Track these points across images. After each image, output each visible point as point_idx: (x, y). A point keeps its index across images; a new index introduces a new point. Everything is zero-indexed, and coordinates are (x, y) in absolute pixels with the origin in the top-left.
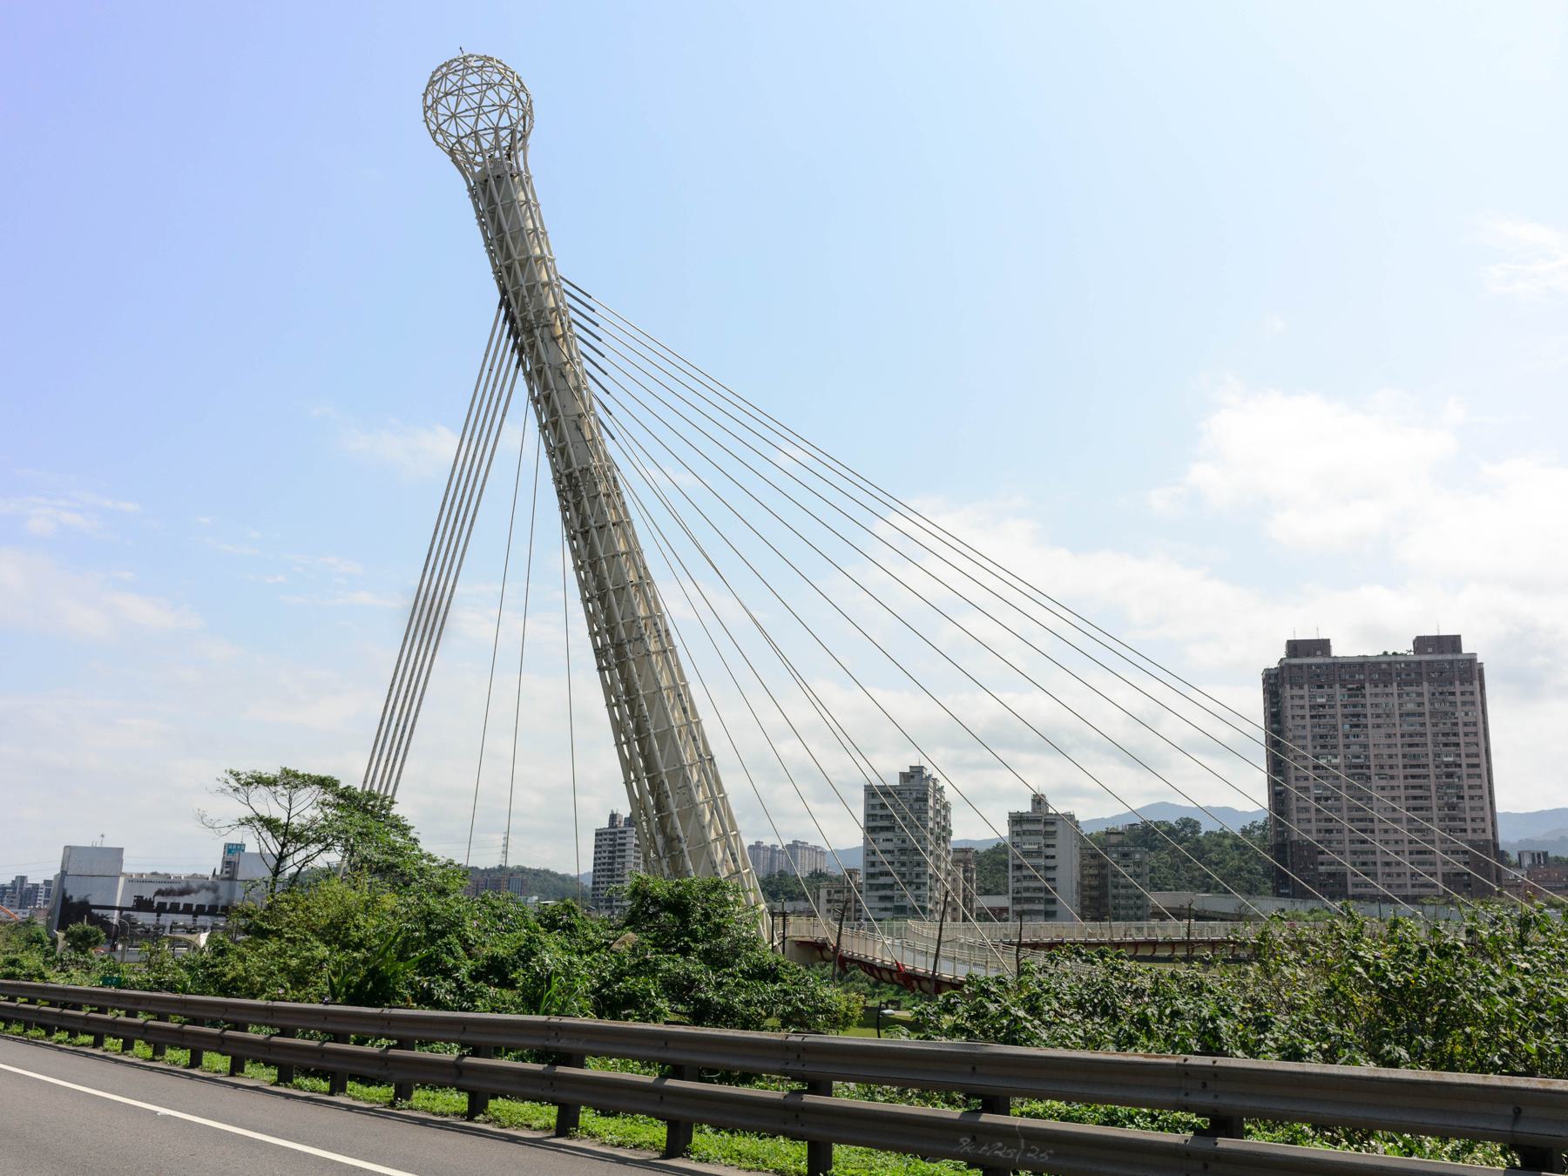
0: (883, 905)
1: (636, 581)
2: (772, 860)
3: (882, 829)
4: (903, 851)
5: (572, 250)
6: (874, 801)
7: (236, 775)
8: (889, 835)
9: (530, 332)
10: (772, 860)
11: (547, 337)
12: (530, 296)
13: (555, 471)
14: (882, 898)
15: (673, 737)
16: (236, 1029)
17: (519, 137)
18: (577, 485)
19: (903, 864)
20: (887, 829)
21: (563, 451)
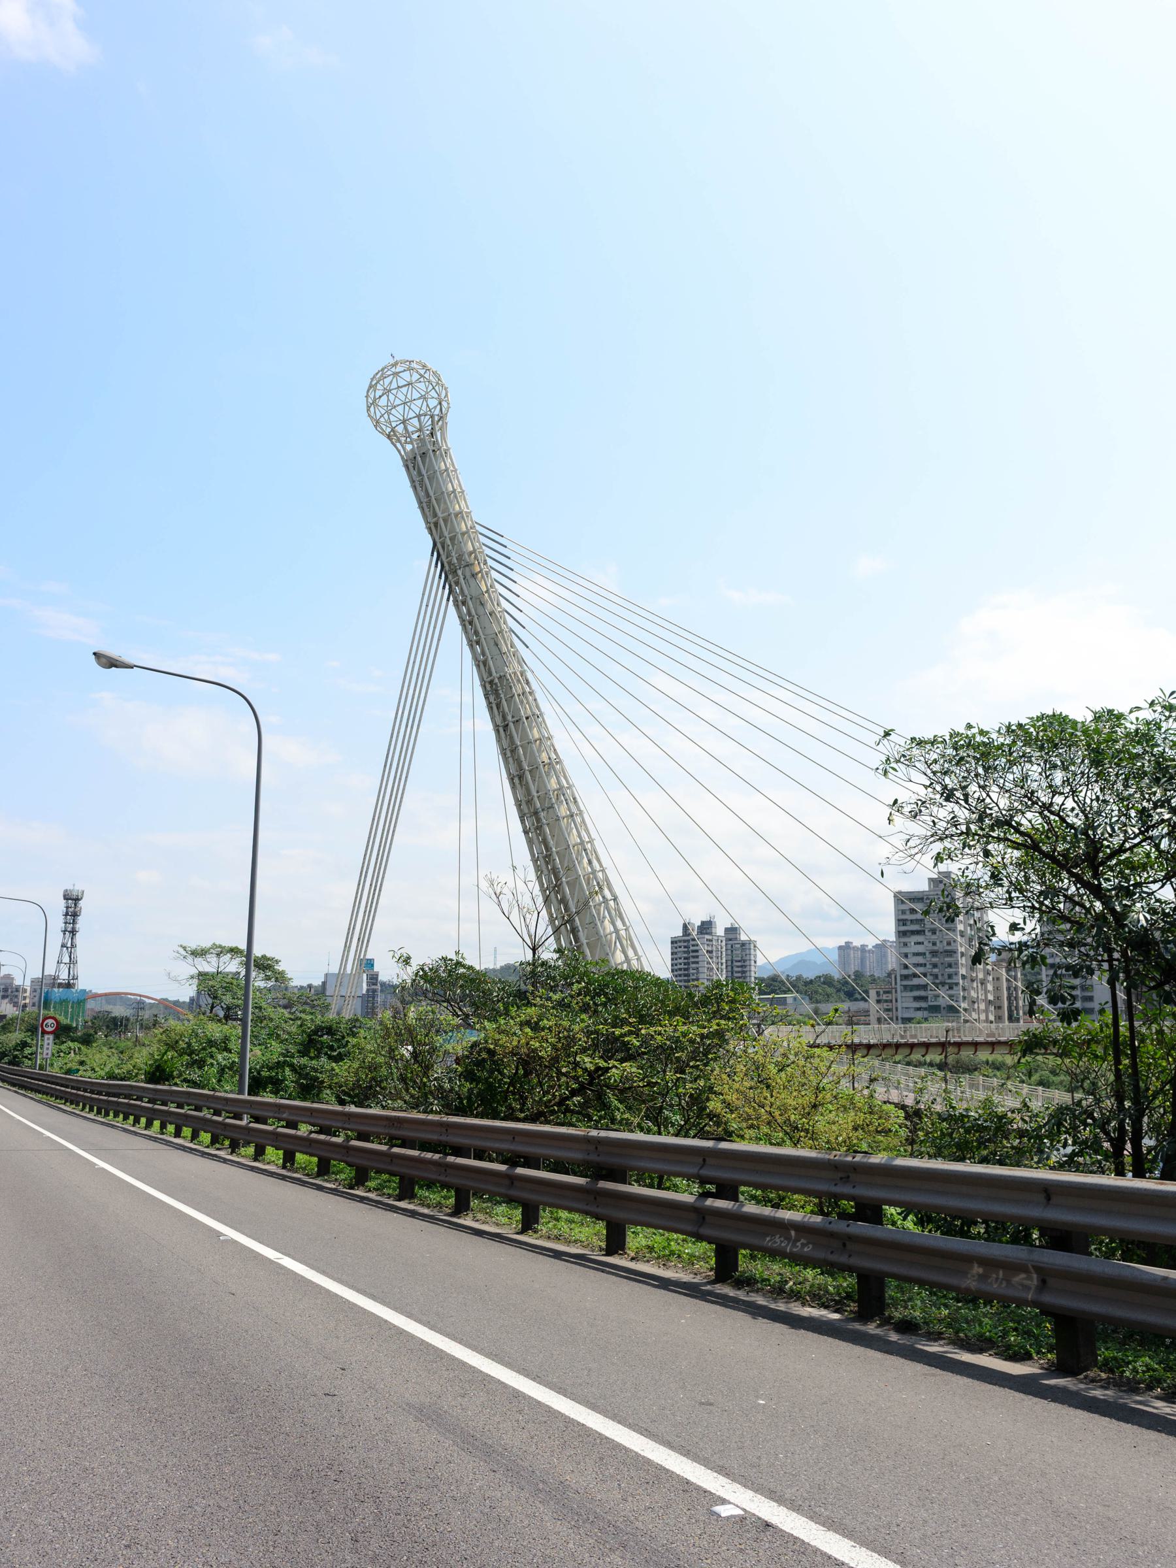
0: (917, 1005)
1: (547, 761)
2: (863, 960)
3: (913, 933)
4: (934, 953)
5: (482, 501)
6: (903, 907)
7: (184, 948)
8: (920, 938)
9: (455, 572)
10: (863, 960)
11: (468, 574)
12: (453, 544)
13: (482, 679)
14: (916, 999)
15: (580, 884)
16: (402, 1146)
17: (439, 419)
18: (497, 690)
19: (935, 966)
20: (918, 933)
21: (485, 663)
